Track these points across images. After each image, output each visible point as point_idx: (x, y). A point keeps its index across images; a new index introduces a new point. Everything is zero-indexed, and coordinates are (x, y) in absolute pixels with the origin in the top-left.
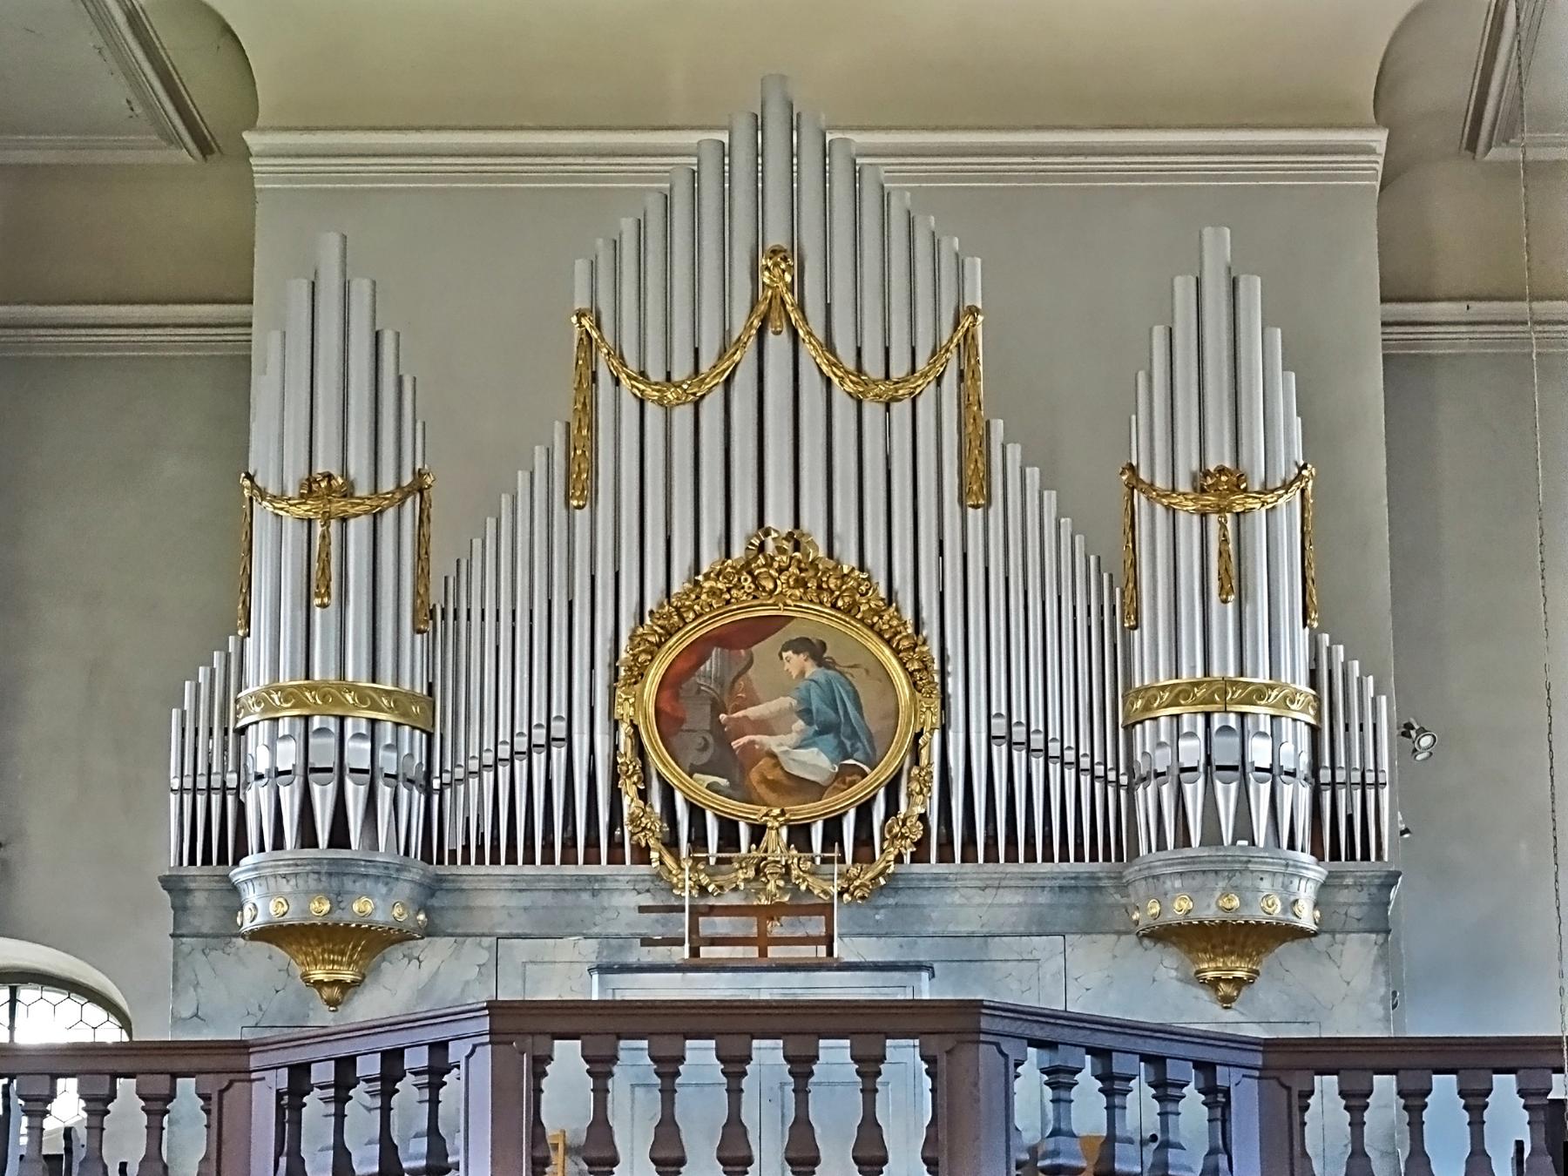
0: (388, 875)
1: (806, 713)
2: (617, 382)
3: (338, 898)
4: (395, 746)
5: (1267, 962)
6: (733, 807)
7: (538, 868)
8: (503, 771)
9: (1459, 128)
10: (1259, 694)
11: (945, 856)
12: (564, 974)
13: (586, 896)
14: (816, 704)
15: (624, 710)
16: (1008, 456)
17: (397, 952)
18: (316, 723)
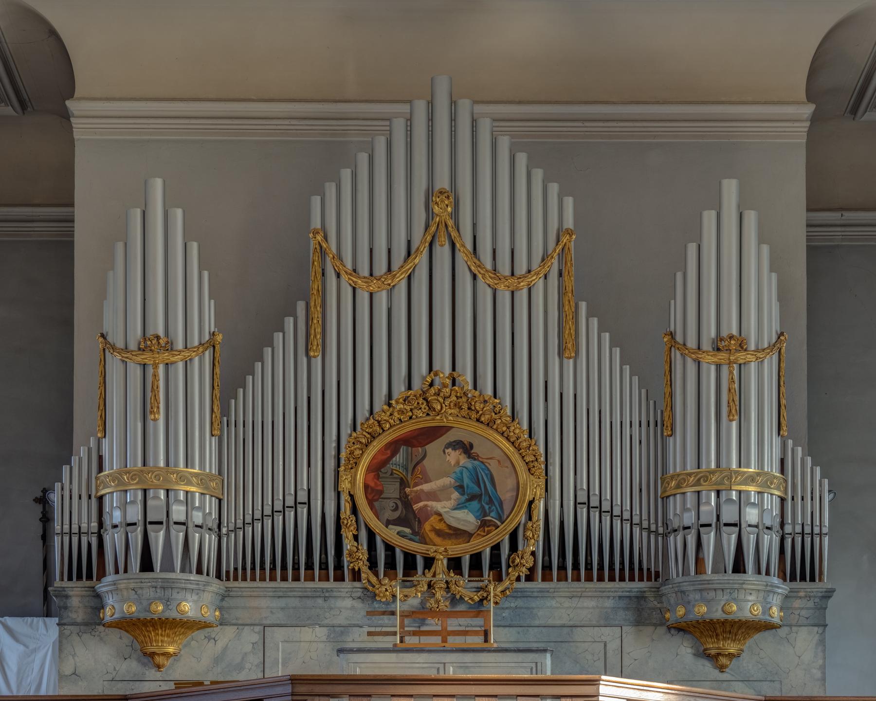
1: (460, 488)
3: (167, 602)
5: (750, 642)
13: (320, 601)
14: (466, 481)
15: (345, 485)
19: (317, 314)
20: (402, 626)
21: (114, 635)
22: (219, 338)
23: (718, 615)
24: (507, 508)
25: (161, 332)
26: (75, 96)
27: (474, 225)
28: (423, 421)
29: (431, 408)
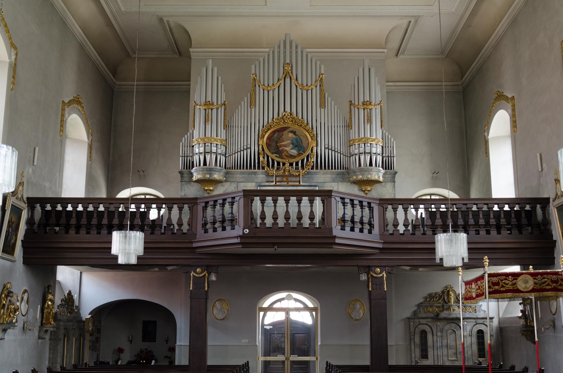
0: (219, 171)
1: (292, 144)
2: (259, 86)
3: (210, 175)
4: (220, 148)
5: (374, 187)
6: (279, 160)
7: (245, 170)
8: (239, 153)
9: (394, 52)
10: (374, 140)
11: (317, 168)
12: (251, 186)
13: (253, 175)
14: (294, 142)
15: (261, 143)
16: (328, 100)
17: (220, 185)
18: (207, 144)
19: (253, 97)
20: (276, 179)
21: (196, 184)
22: (226, 103)
23: (365, 178)
24: (305, 149)
25: (210, 100)
26: (193, 46)
27: (297, 75)
28: (282, 125)
29: (284, 121)
